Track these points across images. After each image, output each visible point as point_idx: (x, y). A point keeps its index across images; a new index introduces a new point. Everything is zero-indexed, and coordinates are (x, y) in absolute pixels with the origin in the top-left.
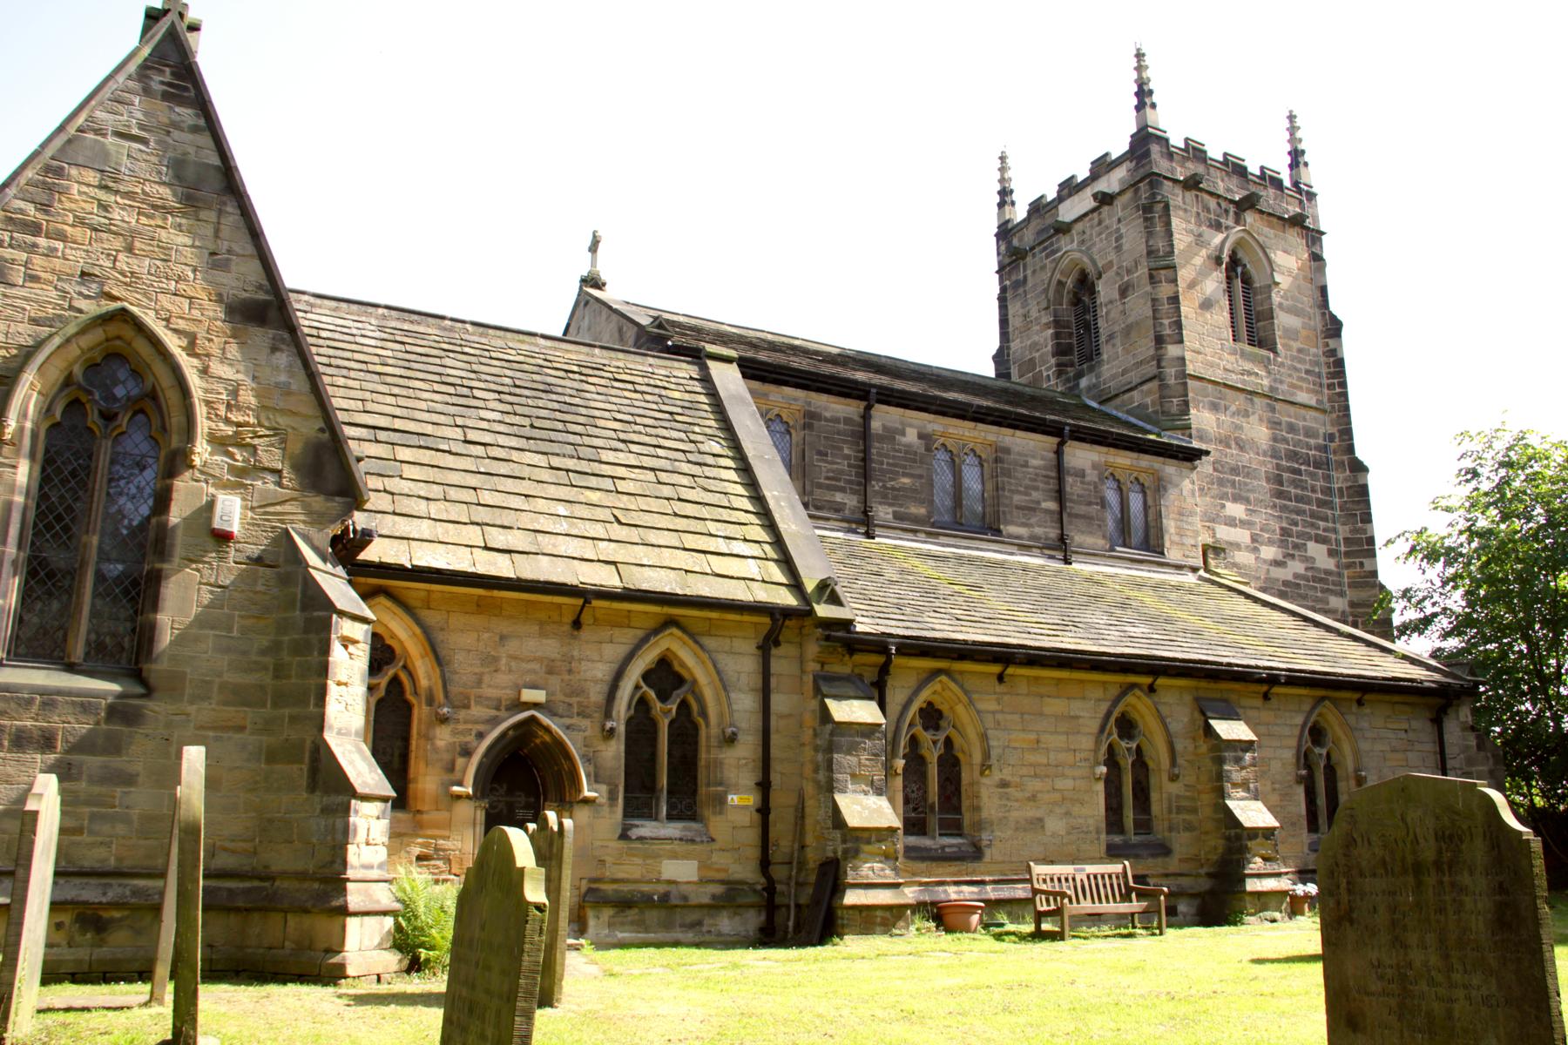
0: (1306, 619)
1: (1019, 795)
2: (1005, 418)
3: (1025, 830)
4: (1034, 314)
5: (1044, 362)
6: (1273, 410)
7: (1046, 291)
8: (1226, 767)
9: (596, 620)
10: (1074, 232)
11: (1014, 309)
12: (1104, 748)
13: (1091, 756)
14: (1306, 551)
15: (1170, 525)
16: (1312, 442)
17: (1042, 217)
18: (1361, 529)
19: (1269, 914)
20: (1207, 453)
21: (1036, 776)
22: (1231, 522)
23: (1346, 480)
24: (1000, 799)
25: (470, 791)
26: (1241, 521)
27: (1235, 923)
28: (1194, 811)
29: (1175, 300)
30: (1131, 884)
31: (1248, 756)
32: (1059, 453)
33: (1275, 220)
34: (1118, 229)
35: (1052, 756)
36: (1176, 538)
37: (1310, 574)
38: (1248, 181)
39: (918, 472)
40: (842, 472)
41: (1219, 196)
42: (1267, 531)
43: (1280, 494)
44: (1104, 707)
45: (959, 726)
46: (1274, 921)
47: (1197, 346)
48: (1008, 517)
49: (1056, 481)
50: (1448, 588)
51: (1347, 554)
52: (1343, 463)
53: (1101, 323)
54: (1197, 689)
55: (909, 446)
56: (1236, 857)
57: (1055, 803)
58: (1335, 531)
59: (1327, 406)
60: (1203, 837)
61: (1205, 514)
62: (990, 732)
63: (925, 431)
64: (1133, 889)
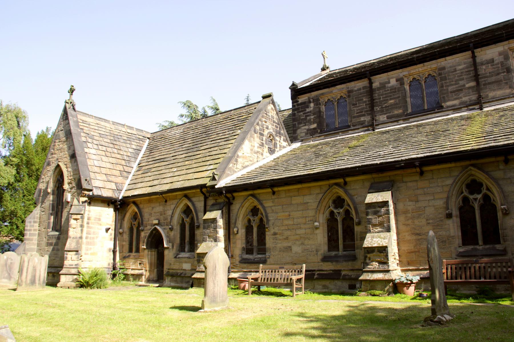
1: (281, 238)
3: (283, 251)
9: (170, 199)
19: (373, 292)
21: (288, 229)
24: (273, 240)
25: (145, 247)
35: (295, 220)
39: (397, 96)
40: (363, 109)
48: (446, 98)
55: (393, 86)
57: (297, 240)
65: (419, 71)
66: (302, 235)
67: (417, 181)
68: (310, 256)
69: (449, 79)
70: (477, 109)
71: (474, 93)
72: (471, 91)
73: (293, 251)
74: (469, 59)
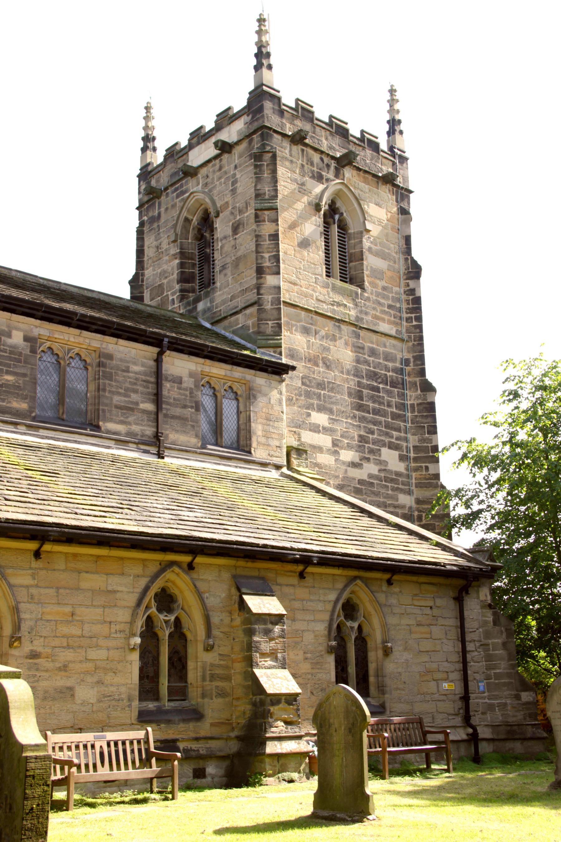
0: (363, 511)
1: (50, 665)
2: (109, 328)
3: (54, 699)
4: (165, 246)
5: (170, 288)
6: (358, 336)
7: (175, 226)
8: (256, 639)
10: (200, 176)
11: (149, 241)
12: (140, 623)
13: (127, 628)
14: (380, 455)
15: (258, 428)
16: (390, 365)
17: (176, 161)
18: (428, 439)
19: (286, 775)
20: (293, 368)
21: (68, 647)
22: (315, 429)
23: (417, 398)
26: (324, 428)
27: (253, 785)
28: (228, 678)
29: (275, 237)
30: (152, 749)
31: (277, 629)
32: (158, 361)
33: (370, 177)
34: (235, 175)
35: (86, 627)
36: (263, 440)
37: (382, 475)
38: (349, 141)
41: (322, 152)
42: (346, 438)
43: (360, 407)
44: (143, 582)
45: (186, 608)
46: (291, 781)
47: (294, 278)
48: (108, 415)
49: (154, 386)
50: (494, 489)
51: (416, 459)
52: (415, 383)
53: (217, 255)
54: (236, 567)
55: (14, 347)
56: (259, 721)
57: (87, 673)
58: (406, 440)
59: (405, 336)
60: (235, 703)
61: (292, 420)
62: (22, 606)
63: (30, 335)
64: (154, 754)
65: (68, 341)
66: (98, 663)
67: (293, 586)
68: (116, 710)
69: (116, 381)
70: (154, 454)
71: (150, 423)
72: (146, 419)
73: (76, 698)
74: (149, 360)
